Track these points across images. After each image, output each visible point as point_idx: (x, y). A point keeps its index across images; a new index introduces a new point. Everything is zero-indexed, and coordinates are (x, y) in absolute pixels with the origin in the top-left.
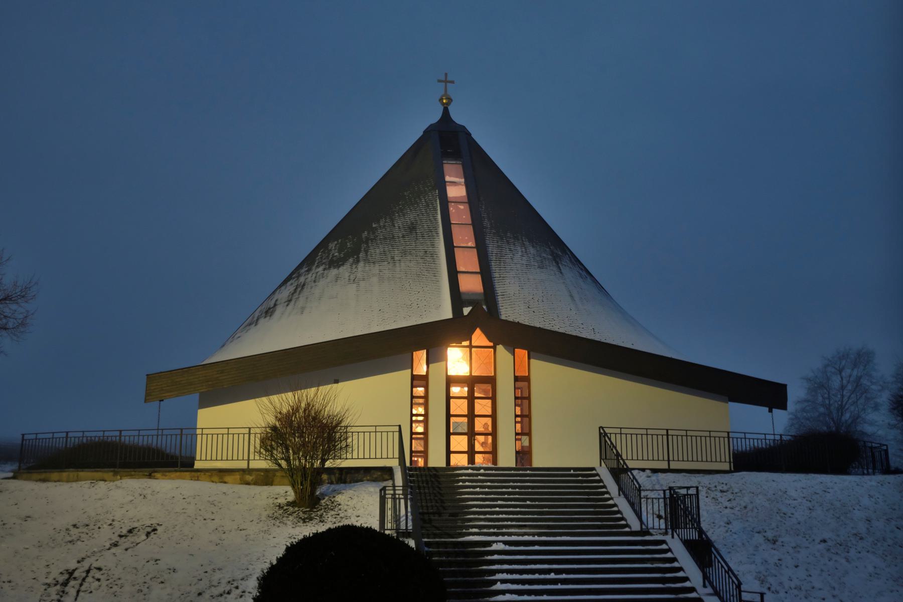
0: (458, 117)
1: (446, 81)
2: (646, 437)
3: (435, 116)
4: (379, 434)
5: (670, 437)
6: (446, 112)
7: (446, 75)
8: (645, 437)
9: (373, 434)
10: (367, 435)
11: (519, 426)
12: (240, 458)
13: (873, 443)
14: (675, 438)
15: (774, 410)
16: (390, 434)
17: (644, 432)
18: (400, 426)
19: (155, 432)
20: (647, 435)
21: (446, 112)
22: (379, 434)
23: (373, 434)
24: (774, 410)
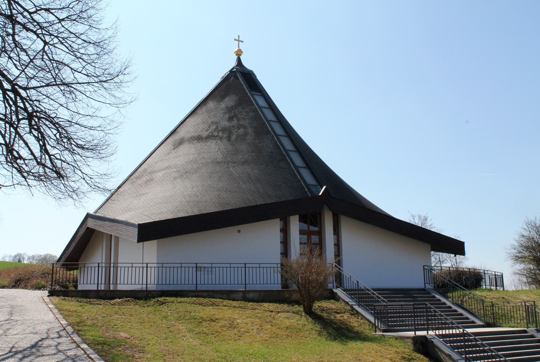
0: (248, 64)
1: (239, 41)
2: (211, 269)
3: (232, 64)
4: (261, 269)
5: (247, 269)
6: (239, 61)
7: (239, 36)
8: (229, 269)
9: (258, 269)
10: (254, 269)
11: (499, 274)
12: (92, 282)
13: (26, 160)
14: (251, 269)
15: (457, 255)
16: (191, 269)
17: (258, 265)
18: (502, 273)
19: (141, 265)
20: (181, 267)
21: (239, 61)
22: (261, 269)
23: (258, 269)
24: (457, 255)
